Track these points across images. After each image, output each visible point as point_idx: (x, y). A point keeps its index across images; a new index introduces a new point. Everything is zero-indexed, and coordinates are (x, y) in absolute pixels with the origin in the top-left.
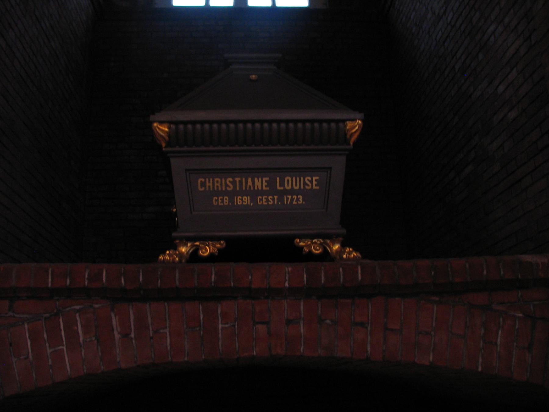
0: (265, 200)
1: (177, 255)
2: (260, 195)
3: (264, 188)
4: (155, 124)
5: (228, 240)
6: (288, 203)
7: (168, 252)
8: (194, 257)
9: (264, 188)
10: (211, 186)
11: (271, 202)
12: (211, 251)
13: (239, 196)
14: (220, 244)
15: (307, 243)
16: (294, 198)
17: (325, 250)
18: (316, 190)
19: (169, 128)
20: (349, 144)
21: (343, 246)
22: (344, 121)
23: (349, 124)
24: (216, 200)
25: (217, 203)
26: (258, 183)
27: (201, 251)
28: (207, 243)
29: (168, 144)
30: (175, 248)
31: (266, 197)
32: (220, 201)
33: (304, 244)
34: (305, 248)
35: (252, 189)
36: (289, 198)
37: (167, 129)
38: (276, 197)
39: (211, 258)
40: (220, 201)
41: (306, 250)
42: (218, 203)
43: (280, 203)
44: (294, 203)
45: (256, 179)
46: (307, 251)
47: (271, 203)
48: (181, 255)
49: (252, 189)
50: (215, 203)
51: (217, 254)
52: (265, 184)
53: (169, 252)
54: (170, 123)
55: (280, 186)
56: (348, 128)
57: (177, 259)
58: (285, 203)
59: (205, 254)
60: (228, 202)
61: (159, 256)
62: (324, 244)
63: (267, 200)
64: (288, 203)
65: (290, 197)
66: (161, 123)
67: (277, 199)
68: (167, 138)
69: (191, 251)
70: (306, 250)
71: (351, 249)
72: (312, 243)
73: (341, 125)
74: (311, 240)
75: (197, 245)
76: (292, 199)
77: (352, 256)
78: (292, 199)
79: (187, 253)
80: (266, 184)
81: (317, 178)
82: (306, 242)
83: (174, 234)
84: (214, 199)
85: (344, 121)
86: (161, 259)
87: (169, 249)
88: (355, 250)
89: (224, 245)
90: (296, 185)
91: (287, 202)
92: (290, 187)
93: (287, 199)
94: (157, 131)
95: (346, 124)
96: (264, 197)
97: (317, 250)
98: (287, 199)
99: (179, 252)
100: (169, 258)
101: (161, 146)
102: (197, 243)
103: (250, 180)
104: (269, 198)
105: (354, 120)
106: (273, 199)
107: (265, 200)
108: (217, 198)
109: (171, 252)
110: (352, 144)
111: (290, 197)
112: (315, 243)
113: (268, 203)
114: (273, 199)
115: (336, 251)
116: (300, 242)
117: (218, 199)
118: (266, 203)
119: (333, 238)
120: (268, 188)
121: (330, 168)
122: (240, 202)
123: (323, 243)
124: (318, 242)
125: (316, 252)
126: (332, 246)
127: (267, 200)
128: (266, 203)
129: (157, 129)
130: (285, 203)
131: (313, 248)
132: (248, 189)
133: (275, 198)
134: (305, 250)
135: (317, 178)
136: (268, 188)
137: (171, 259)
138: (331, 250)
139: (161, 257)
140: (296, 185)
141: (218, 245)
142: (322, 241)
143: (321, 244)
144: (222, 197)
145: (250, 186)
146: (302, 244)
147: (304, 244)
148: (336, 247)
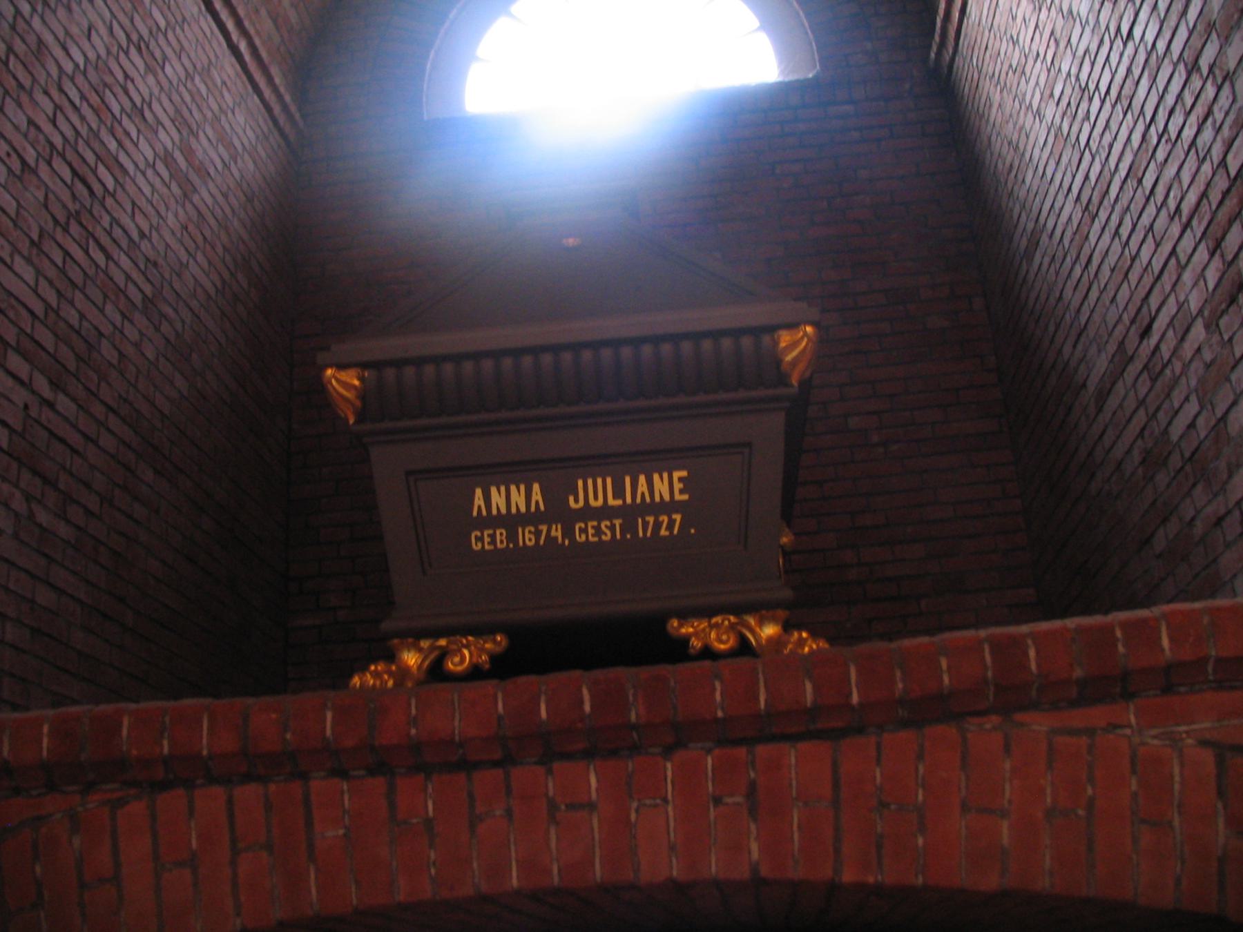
0: (593, 531)
1: (390, 673)
2: (476, 529)
3: (678, 497)
4: (329, 372)
5: (511, 631)
6: (649, 534)
7: (373, 668)
8: (436, 671)
9: (678, 497)
10: (573, 502)
11: (606, 535)
12: (474, 660)
13: (529, 525)
14: (494, 641)
15: (698, 626)
16: (663, 521)
17: (743, 641)
18: (612, 507)
19: (361, 379)
20: (792, 386)
21: (787, 627)
22: (772, 329)
23: (785, 338)
24: (581, 530)
25: (480, 545)
26: (661, 487)
27: (451, 663)
28: (464, 641)
29: (361, 417)
30: (391, 656)
31: (595, 523)
32: (487, 539)
33: (691, 630)
34: (693, 639)
35: (484, 513)
36: (648, 522)
37: (356, 383)
38: (617, 522)
39: (475, 673)
40: (487, 539)
41: (696, 643)
42: (587, 537)
43: (628, 536)
44: (664, 532)
45: (494, 490)
46: (700, 645)
47: (607, 537)
48: (404, 671)
49: (484, 513)
50: (477, 547)
51: (487, 666)
52: (678, 486)
53: (376, 667)
54: (364, 366)
55: (614, 498)
56: (783, 345)
57: (390, 683)
58: (641, 534)
59: (460, 668)
60: (505, 541)
61: (351, 677)
62: (739, 627)
63: (598, 532)
64: (649, 534)
65: (651, 519)
66: (341, 367)
67: (621, 525)
68: (358, 403)
69: (427, 663)
70: (696, 643)
71: (804, 635)
72: (711, 627)
73: (766, 339)
74: (707, 620)
75: (441, 647)
76: (658, 525)
77: (806, 649)
78: (658, 525)
79: (419, 667)
80: (681, 486)
81: (684, 473)
82: (695, 624)
83: (386, 626)
84: (577, 527)
85: (772, 329)
86: (355, 685)
87: (375, 660)
88: (814, 634)
89: (504, 643)
90: (596, 498)
91: (645, 531)
92: (581, 503)
93: (645, 524)
94: (334, 388)
95: (776, 336)
96: (590, 524)
97: (721, 642)
98: (645, 524)
99: (398, 667)
100: (801, 634)
101: (347, 420)
102: (443, 642)
103: (642, 479)
104: (603, 526)
105: (792, 326)
106: (612, 528)
107: (593, 531)
108: (583, 525)
109: (821, 644)
110: (795, 382)
111: (651, 519)
112: (717, 625)
113: (600, 538)
114: (612, 528)
115: (770, 639)
116: (681, 625)
117: (483, 534)
118: (596, 539)
119: (762, 609)
120: (685, 497)
121: (749, 445)
122: (530, 540)
123: (737, 624)
124: (726, 623)
125: (722, 647)
126: (758, 630)
127: (598, 532)
128: (596, 539)
129: (333, 381)
130: (641, 534)
131: (466, 658)
132: (638, 500)
133: (615, 525)
134: (693, 644)
135: (684, 473)
136: (685, 497)
137: (378, 683)
138: (756, 640)
139: (356, 680)
140: (596, 498)
141: (488, 646)
142: (732, 618)
143: (732, 626)
144: (491, 532)
145: (643, 494)
146: (687, 630)
147: (691, 630)
148: (769, 630)
